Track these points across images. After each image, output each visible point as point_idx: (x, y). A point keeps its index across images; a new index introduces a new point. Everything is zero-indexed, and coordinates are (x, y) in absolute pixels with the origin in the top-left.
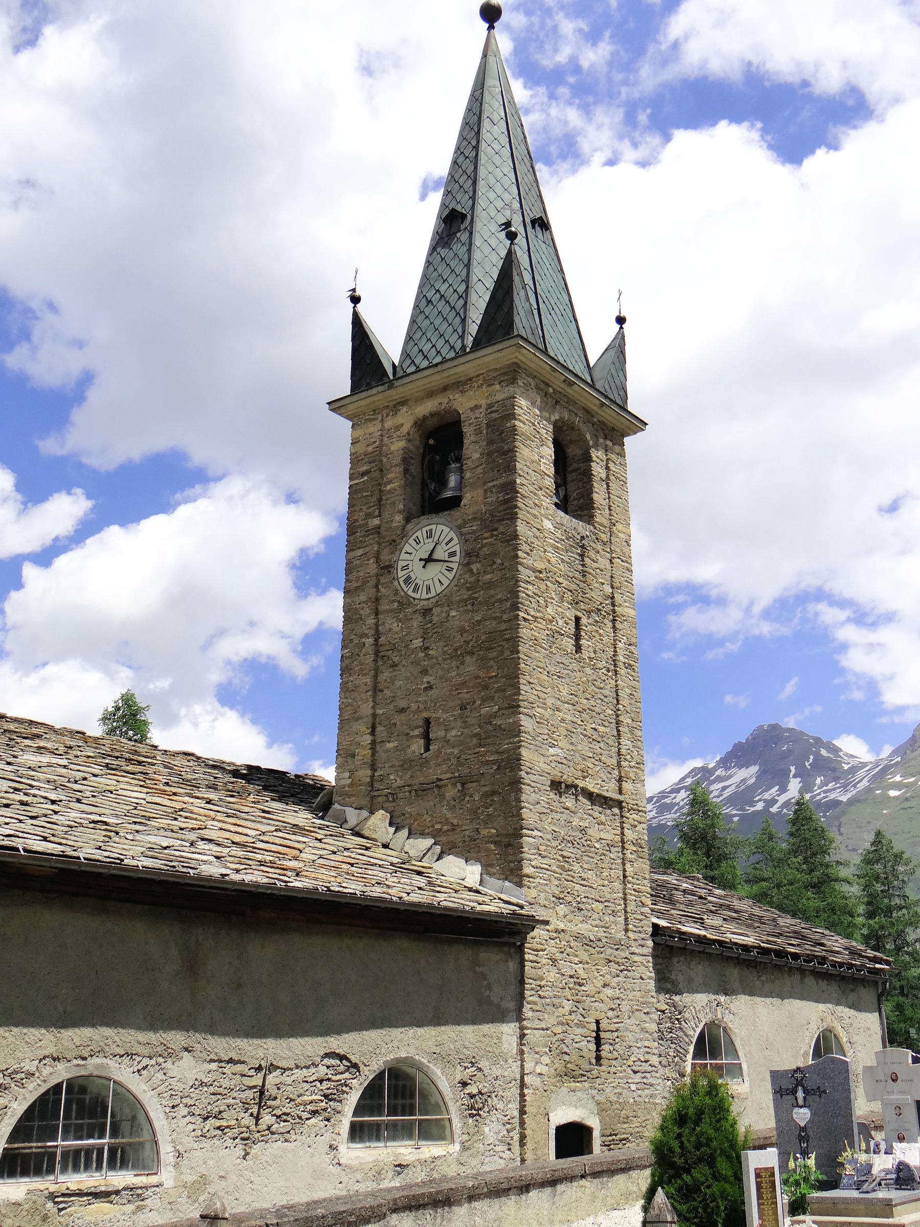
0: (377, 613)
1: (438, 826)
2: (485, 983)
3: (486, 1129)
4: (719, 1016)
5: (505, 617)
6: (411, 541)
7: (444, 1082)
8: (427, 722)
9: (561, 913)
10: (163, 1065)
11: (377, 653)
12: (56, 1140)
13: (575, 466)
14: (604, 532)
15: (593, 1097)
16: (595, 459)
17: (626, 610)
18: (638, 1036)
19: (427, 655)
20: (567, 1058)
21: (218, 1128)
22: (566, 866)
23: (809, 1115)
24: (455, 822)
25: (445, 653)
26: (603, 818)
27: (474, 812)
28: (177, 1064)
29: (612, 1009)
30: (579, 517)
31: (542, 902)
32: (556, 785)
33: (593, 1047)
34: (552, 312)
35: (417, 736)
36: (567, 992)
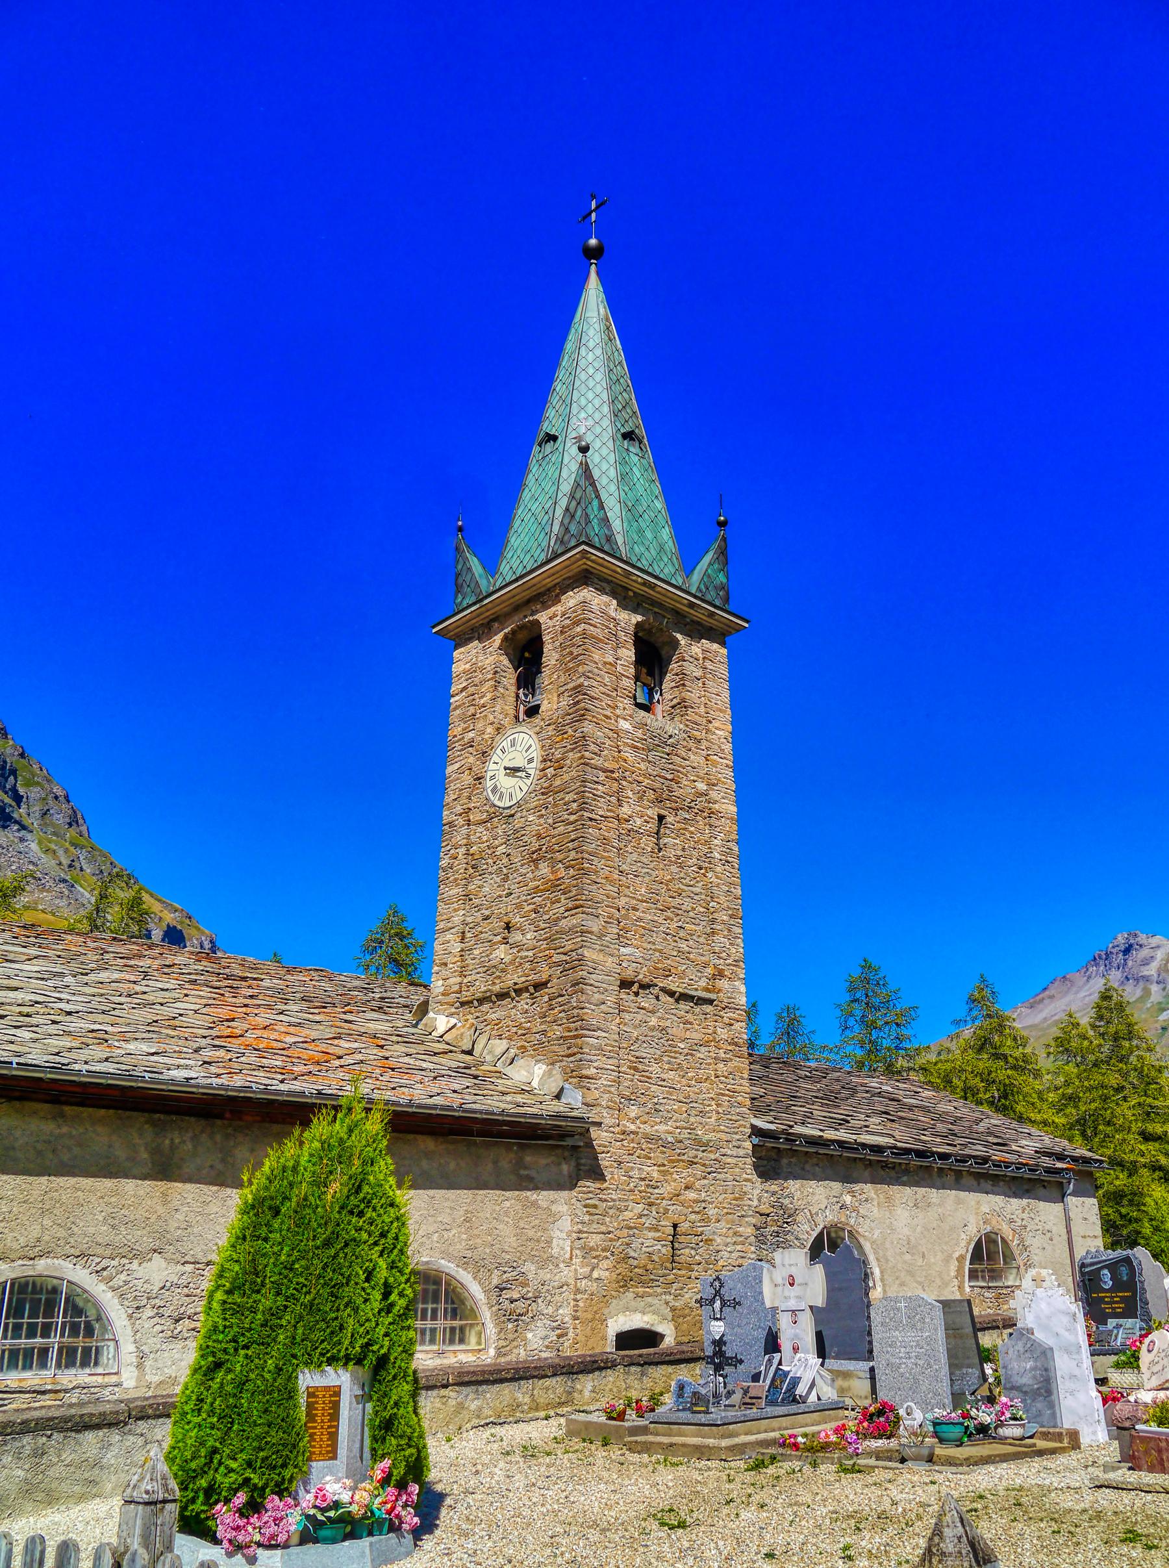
3: (530, 1335)
6: (498, 751)
15: (667, 1303)
21: (193, 1330)
28: (144, 1264)
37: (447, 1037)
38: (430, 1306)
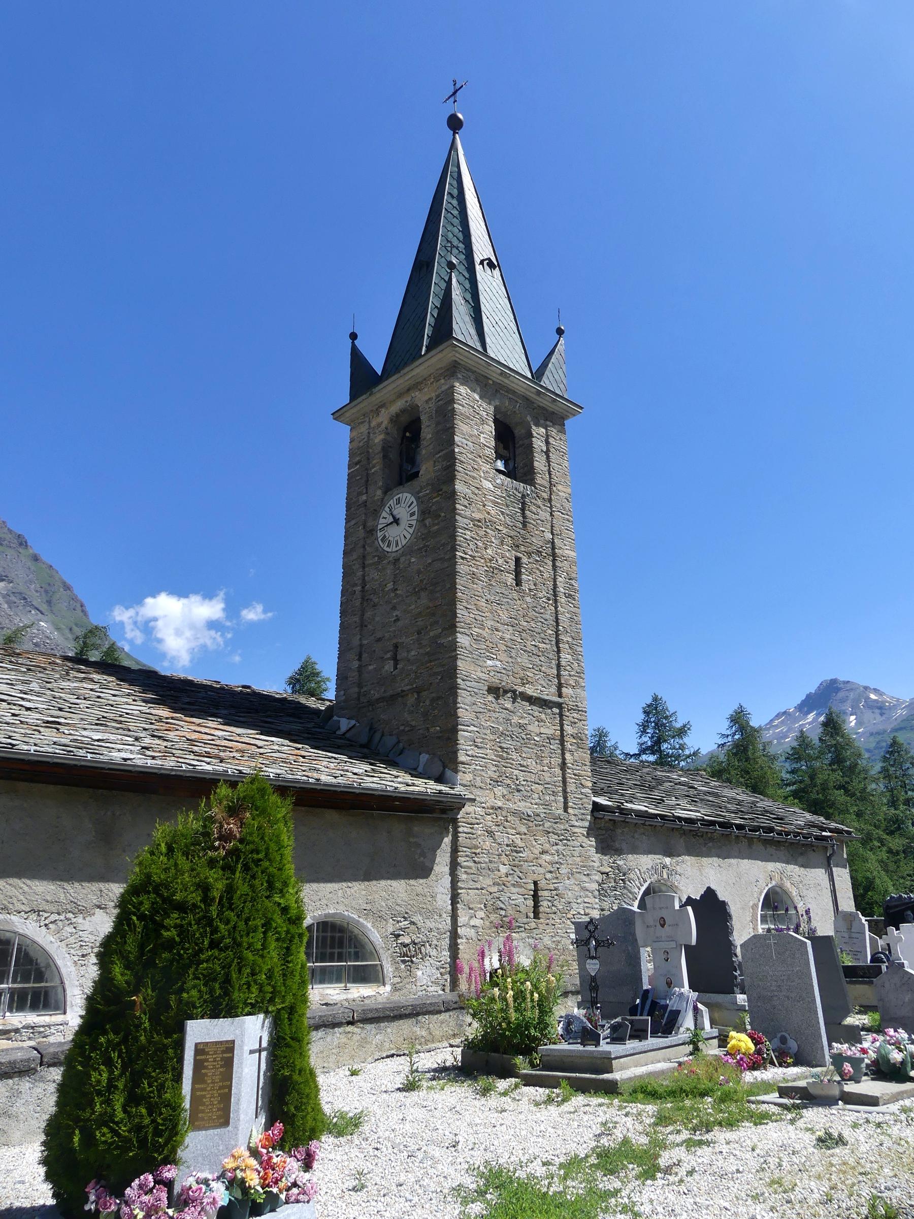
0: (364, 568)
1: (402, 728)
2: (419, 851)
3: (419, 973)
4: (665, 876)
5: (447, 557)
7: (376, 934)
8: (396, 646)
9: (499, 794)
10: (74, 920)
11: (363, 598)
12: (29, 983)
13: (521, 442)
14: (545, 492)
16: (535, 435)
17: (567, 552)
18: (577, 894)
19: (396, 595)
20: (503, 913)
22: (505, 755)
23: (598, 966)
24: (413, 723)
25: (408, 591)
26: (543, 716)
27: (425, 714)
29: (551, 872)
30: (524, 482)
31: (479, 784)
32: (495, 691)
33: (531, 903)
34: (496, 326)
35: (389, 659)
36: (504, 859)
37: (348, 735)
38: (336, 951)
